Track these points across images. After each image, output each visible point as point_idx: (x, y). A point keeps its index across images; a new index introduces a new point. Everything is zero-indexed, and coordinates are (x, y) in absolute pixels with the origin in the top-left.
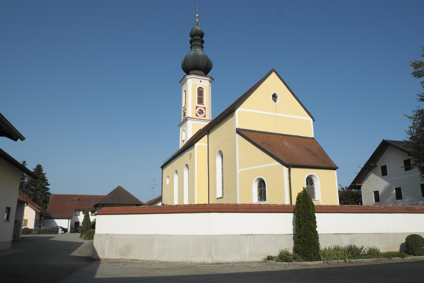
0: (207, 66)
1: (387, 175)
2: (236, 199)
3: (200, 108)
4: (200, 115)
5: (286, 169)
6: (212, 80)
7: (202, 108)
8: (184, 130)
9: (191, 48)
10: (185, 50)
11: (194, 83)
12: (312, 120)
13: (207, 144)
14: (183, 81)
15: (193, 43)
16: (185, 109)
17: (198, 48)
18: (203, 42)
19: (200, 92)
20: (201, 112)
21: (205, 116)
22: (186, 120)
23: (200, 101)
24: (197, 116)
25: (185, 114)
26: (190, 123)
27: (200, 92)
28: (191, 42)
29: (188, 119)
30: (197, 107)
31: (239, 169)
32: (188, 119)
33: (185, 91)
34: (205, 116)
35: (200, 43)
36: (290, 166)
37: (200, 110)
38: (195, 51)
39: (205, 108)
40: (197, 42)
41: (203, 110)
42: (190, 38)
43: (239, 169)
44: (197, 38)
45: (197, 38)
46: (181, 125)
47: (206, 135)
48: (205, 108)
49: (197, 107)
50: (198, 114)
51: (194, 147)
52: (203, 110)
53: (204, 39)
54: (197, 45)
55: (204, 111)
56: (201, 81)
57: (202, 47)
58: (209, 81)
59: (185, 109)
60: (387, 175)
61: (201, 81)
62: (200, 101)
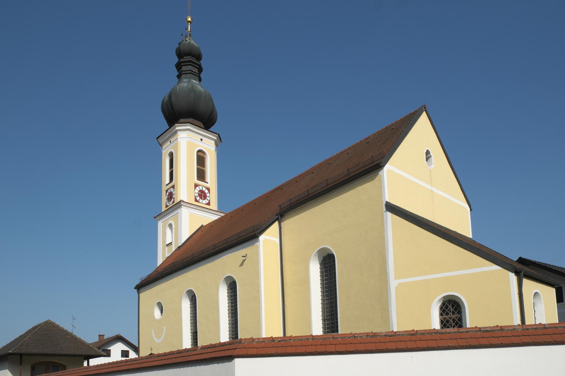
0: (211, 115)
1: (563, 302)
2: (219, 337)
3: (201, 188)
4: (201, 201)
5: (513, 278)
6: (219, 142)
7: (204, 189)
8: (170, 226)
9: (179, 77)
10: (166, 81)
11: (188, 141)
12: (469, 209)
13: (278, 240)
14: (162, 138)
15: (184, 68)
16: (173, 187)
17: (194, 79)
18: (200, 70)
19: (201, 159)
20: (202, 195)
21: (209, 204)
22: (179, 205)
23: (201, 175)
24: (196, 200)
25: (170, 196)
26: (185, 212)
27: (201, 159)
28: (179, 66)
29: (182, 203)
30: (196, 186)
31: (395, 279)
32: (182, 203)
33: (171, 155)
34: (209, 204)
35: (196, 70)
36: (522, 274)
37: (201, 191)
38: (188, 82)
39: (208, 189)
40: (190, 68)
41: (206, 191)
42: (176, 60)
43: (395, 279)
44: (189, 60)
45: (189, 60)
46: (160, 215)
47: (277, 223)
48: (208, 189)
49: (196, 186)
50: (198, 198)
51: (258, 241)
52: (206, 191)
53: (203, 62)
54: (192, 73)
55: (208, 195)
56: (201, 140)
57: (200, 80)
58: (215, 141)
59: (173, 187)
60: (563, 302)
61: (201, 140)
62: (201, 175)
